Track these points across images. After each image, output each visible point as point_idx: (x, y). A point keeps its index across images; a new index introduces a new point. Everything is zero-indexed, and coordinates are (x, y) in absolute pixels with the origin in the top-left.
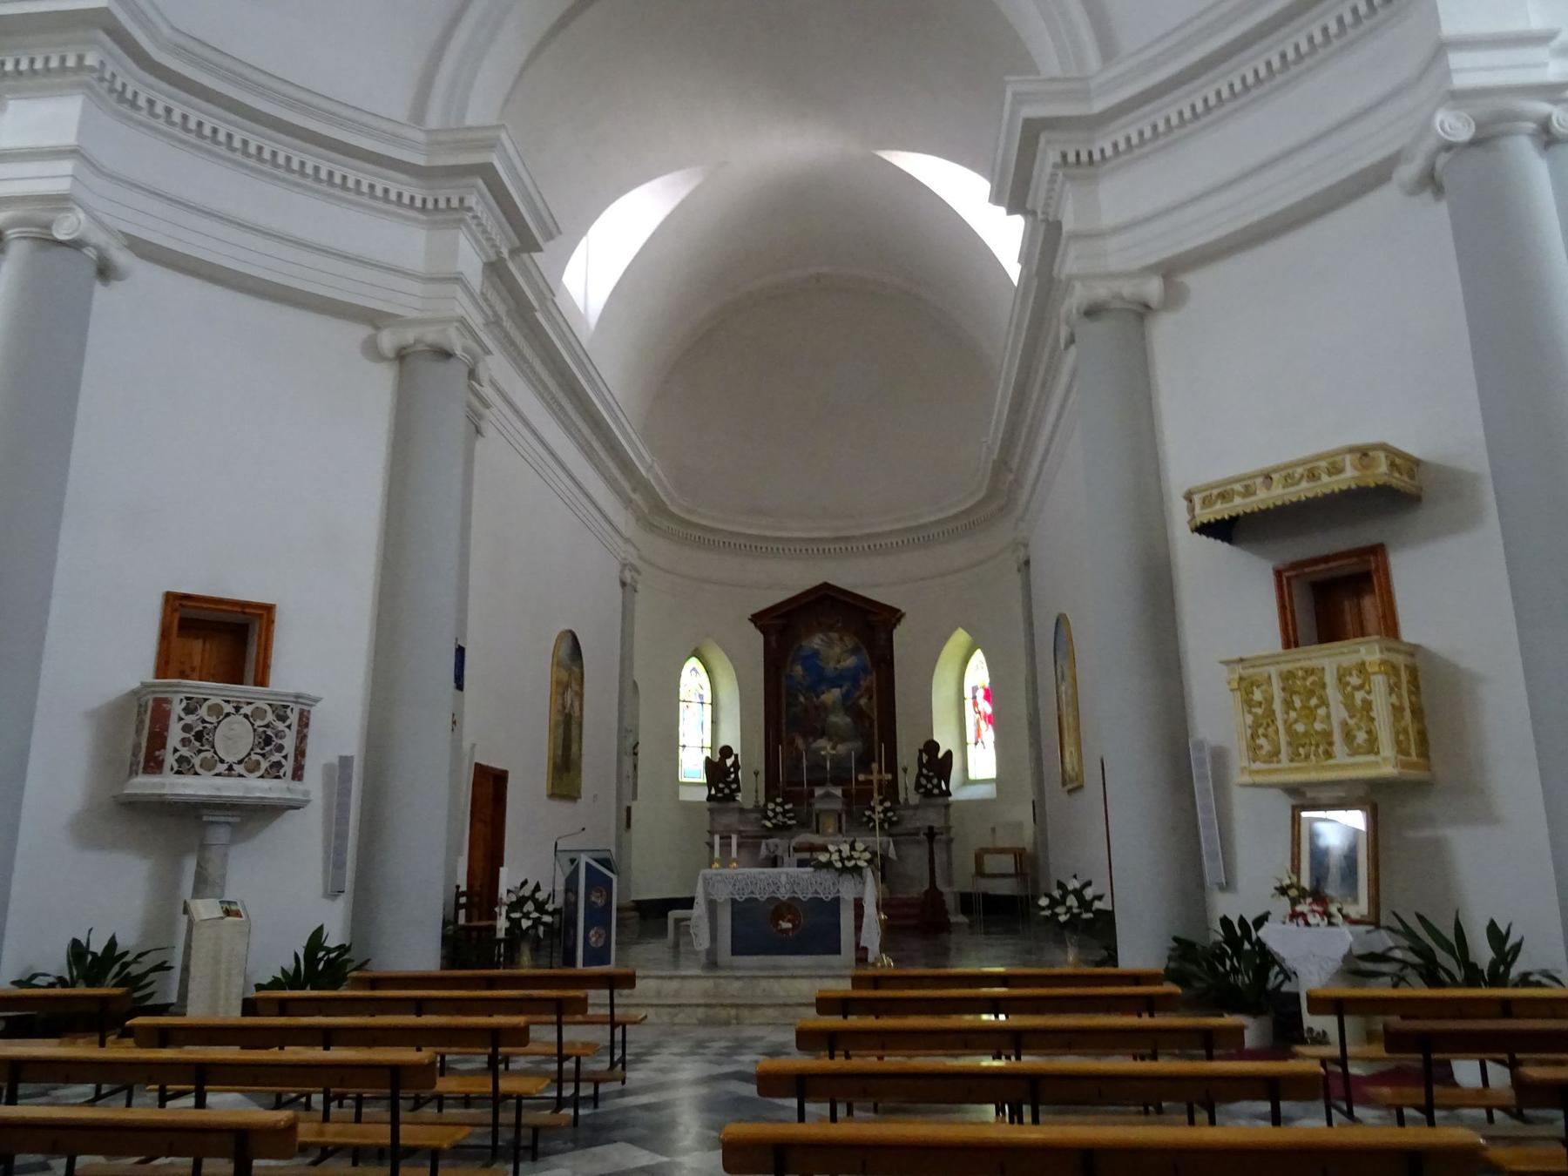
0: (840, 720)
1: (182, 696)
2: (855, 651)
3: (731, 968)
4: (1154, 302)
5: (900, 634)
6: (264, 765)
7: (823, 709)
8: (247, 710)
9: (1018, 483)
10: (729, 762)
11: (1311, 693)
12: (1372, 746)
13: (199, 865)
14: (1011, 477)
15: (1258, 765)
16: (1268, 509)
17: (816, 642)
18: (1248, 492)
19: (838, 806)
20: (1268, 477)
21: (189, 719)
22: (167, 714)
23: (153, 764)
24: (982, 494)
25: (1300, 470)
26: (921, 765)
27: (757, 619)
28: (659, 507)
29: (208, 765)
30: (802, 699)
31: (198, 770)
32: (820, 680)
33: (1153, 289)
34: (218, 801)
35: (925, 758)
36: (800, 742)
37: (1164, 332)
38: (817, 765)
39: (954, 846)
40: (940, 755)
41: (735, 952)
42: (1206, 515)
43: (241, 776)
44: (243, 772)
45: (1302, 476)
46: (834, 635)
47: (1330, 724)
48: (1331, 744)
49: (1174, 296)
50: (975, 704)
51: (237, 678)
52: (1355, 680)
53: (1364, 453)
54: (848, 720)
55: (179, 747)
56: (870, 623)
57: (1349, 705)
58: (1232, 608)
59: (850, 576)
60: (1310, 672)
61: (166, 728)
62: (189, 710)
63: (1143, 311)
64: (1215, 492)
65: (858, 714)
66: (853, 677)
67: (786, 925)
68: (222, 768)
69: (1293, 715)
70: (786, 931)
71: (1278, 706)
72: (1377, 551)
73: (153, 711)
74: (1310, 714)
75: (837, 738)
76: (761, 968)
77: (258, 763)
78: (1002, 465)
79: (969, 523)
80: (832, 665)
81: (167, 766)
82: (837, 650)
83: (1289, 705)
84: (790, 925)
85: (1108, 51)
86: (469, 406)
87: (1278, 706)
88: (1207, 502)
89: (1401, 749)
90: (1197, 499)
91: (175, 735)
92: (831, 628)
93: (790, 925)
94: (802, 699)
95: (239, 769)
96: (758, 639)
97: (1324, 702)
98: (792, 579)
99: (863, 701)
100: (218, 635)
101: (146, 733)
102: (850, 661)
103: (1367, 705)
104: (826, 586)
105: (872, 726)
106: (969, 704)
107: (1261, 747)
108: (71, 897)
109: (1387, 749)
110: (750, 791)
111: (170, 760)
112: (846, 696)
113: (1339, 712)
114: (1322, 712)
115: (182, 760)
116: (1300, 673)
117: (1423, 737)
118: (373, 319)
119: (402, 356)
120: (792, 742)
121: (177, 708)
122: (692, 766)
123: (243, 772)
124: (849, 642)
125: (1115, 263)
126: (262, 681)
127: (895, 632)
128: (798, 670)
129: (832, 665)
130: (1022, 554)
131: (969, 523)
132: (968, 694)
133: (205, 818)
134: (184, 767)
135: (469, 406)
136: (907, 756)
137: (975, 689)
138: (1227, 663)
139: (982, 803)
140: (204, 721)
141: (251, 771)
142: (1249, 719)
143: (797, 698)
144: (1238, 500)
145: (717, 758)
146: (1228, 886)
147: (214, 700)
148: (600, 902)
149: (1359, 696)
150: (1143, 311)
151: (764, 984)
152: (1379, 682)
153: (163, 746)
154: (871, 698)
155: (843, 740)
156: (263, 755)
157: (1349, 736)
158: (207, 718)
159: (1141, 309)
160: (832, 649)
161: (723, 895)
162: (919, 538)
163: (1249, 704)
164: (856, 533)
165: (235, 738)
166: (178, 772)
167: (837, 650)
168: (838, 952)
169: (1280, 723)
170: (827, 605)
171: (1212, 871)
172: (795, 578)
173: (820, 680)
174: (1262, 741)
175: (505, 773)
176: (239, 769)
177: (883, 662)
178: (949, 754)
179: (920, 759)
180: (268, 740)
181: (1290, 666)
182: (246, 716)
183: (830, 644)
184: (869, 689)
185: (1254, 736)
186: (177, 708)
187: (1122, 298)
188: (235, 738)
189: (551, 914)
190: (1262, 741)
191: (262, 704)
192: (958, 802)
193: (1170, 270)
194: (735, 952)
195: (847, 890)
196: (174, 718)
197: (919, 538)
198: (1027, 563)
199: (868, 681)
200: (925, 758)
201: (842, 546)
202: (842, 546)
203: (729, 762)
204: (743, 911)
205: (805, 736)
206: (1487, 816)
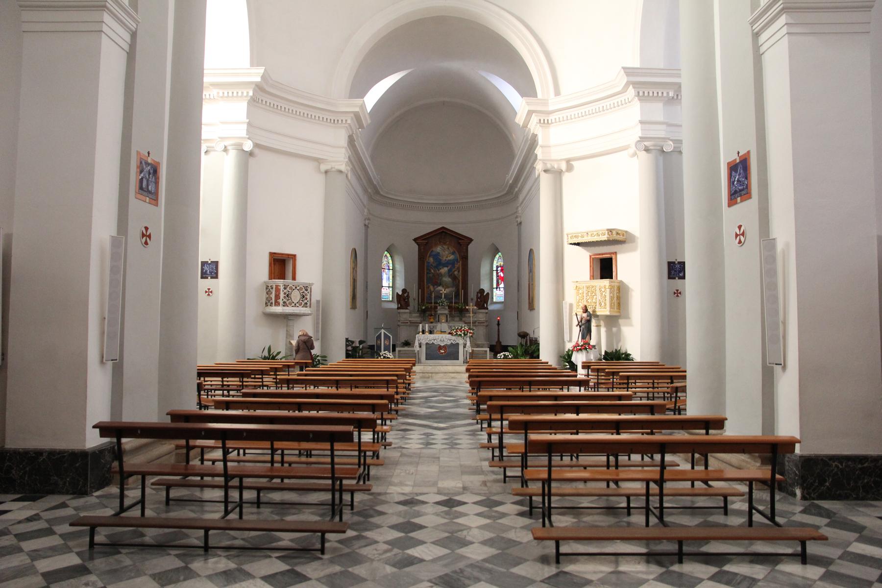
0: (447, 279)
2: (453, 253)
5: (471, 247)
7: (441, 275)
9: (520, 190)
17: (438, 249)
19: (447, 312)
23: (277, 304)
26: (477, 298)
28: (377, 192)
29: (290, 304)
32: (440, 264)
33: (564, 166)
36: (431, 288)
37: (566, 177)
38: (439, 296)
46: (446, 247)
49: (570, 168)
51: (282, 276)
53: (610, 231)
58: (578, 264)
62: (285, 288)
63: (560, 173)
65: (454, 278)
66: (451, 263)
72: (616, 253)
75: (446, 287)
83: (587, 294)
85: (557, 93)
86: (136, 11)
89: (611, 307)
91: (282, 295)
92: (445, 244)
98: (429, 223)
99: (456, 273)
100: (281, 264)
101: (272, 297)
102: (452, 257)
104: (443, 228)
106: (495, 273)
110: (413, 303)
117: (619, 304)
118: (318, 161)
119: (326, 172)
120: (428, 287)
121: (282, 288)
122: (387, 293)
126: (294, 278)
128: (431, 260)
132: (495, 269)
134: (285, 304)
135: (136, 11)
136: (472, 294)
137: (497, 267)
139: (498, 311)
150: (560, 173)
152: (608, 290)
155: (448, 287)
160: (444, 252)
161: (424, 342)
162: (479, 205)
163: (578, 294)
165: (296, 296)
170: (443, 234)
173: (440, 264)
177: (465, 258)
178: (488, 294)
184: (458, 268)
186: (282, 288)
188: (296, 296)
192: (101, 38)
193: (568, 161)
195: (461, 341)
197: (479, 205)
198: (521, 223)
201: (445, 207)
202: (445, 207)
206: (631, 325)
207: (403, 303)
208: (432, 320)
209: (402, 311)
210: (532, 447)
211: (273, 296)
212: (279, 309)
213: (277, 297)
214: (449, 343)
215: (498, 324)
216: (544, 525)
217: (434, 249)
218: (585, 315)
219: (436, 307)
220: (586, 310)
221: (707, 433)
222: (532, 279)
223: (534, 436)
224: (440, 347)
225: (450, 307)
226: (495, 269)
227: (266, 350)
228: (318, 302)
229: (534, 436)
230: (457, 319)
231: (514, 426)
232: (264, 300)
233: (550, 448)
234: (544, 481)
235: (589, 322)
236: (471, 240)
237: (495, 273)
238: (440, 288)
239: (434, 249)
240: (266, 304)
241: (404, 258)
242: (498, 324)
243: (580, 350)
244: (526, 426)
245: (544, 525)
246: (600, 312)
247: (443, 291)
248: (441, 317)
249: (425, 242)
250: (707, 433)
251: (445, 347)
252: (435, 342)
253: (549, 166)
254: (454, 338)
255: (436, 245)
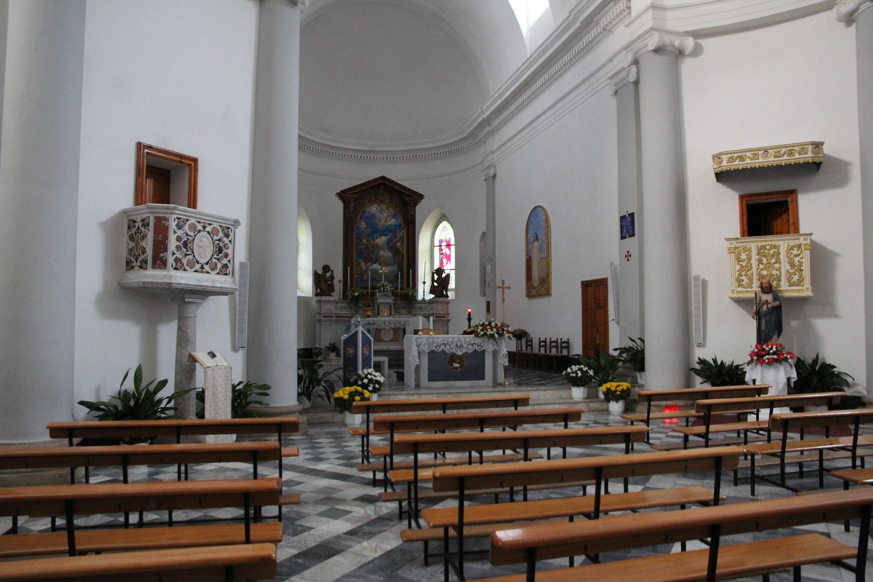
0: (386, 254)
1: (175, 216)
2: (394, 216)
3: (427, 388)
4: (687, 52)
6: (219, 266)
7: (377, 247)
8: (209, 228)
9: (492, 133)
10: (328, 274)
11: (773, 256)
12: (800, 282)
13: (180, 329)
14: (489, 129)
15: (740, 289)
16: (764, 167)
17: (374, 209)
18: (755, 156)
19: (390, 300)
20: (766, 151)
21: (180, 233)
22: (166, 229)
23: (159, 262)
24: (464, 135)
25: (784, 150)
27: (342, 195)
30: (365, 241)
31: (187, 268)
33: (689, 43)
34: (200, 288)
35: (436, 277)
36: (363, 265)
37: (688, 66)
38: (376, 278)
39: (450, 324)
40: (444, 275)
41: (430, 380)
42: (725, 165)
43: (208, 272)
44: (209, 270)
45: (785, 153)
46: (384, 206)
47: (780, 272)
48: (780, 281)
49: (697, 51)
50: (441, 250)
52: (795, 252)
54: (390, 254)
55: (175, 251)
56: (404, 202)
57: (792, 264)
58: (718, 216)
59: (403, 175)
60: (775, 247)
61: (166, 238)
62: (180, 227)
63: (680, 53)
64: (736, 155)
65: (396, 252)
67: (457, 365)
68: (198, 267)
69: (761, 266)
70: (456, 368)
71: (754, 262)
72: (793, 192)
73: (155, 224)
74: (769, 266)
76: (442, 388)
77: (216, 264)
78: (487, 121)
79: (450, 151)
80: (382, 223)
81: (169, 265)
82: (385, 214)
83: (760, 262)
84: (458, 365)
87: (754, 262)
88: (731, 160)
90: (725, 158)
91: (172, 243)
92: (382, 202)
93: (458, 365)
94: (365, 241)
95: (207, 268)
96: (340, 205)
97: (778, 261)
99: (398, 244)
100: (164, 175)
102: (393, 222)
103: (801, 264)
104: (383, 178)
105: (403, 258)
106: (436, 250)
107: (743, 281)
108: (98, 356)
109: (807, 284)
111: (171, 260)
112: (389, 241)
113: (785, 266)
114: (777, 266)
115: (177, 260)
116: (768, 247)
121: (173, 225)
123: (209, 270)
124: (392, 211)
125: (671, 25)
127: (417, 207)
128: (363, 225)
129: (382, 223)
130: (491, 174)
131: (450, 151)
132: (436, 243)
133: (186, 300)
134: (179, 266)
137: (441, 241)
138: (727, 239)
140: (187, 235)
141: (213, 270)
142: (738, 267)
143: (361, 240)
144: (748, 161)
145: (320, 272)
146: (567, 344)
147: (192, 221)
148: (367, 353)
149: (796, 259)
150: (680, 53)
151: (320, 415)
153: (166, 250)
154: (402, 243)
155: (387, 265)
156: (218, 259)
157: (789, 279)
158: (189, 233)
159: (677, 53)
160: (382, 214)
163: (739, 260)
164: (379, 149)
165: (203, 247)
166: (176, 269)
167: (385, 214)
168: (483, 378)
169: (754, 270)
171: (695, 337)
172: (371, 173)
173: (375, 231)
174: (744, 278)
175: (582, 282)
176: (207, 268)
179: (433, 277)
180: (220, 250)
181: (763, 244)
182: (209, 233)
183: (381, 212)
185: (740, 275)
187: (673, 46)
188: (203, 247)
189: (774, 353)
190: (744, 278)
191: (216, 225)
193: (697, 35)
194: (430, 380)
196: (171, 231)
198: (494, 177)
199: (402, 233)
200: (436, 277)
203: (328, 274)
204: (433, 356)
205: (366, 263)
207: (324, 286)
208: (369, 313)
209: (324, 298)
210: (396, 448)
211: (148, 244)
212: (152, 276)
213: (160, 245)
214: (471, 349)
215: (469, 319)
216: (410, 526)
217: (367, 210)
218: (768, 297)
219: (373, 295)
220: (767, 288)
221: (566, 427)
222: (199, 294)
223: (398, 437)
224: (453, 357)
225: (394, 294)
226: (436, 243)
227: (131, 377)
228: (242, 265)
229: (398, 437)
230: (404, 311)
231: (381, 426)
232: (124, 254)
233: (416, 448)
234: (409, 483)
235: (778, 310)
236: (421, 197)
237: (436, 250)
238: (376, 266)
239: (367, 210)
240: (129, 266)
241: (311, 221)
242: (469, 319)
243: (778, 361)
244: (392, 426)
245: (410, 526)
246: (787, 290)
247: (384, 270)
248: (382, 308)
249: (355, 199)
250: (566, 427)
251: (460, 359)
252: (447, 349)
253: (667, 39)
254: (478, 341)
255: (371, 202)
